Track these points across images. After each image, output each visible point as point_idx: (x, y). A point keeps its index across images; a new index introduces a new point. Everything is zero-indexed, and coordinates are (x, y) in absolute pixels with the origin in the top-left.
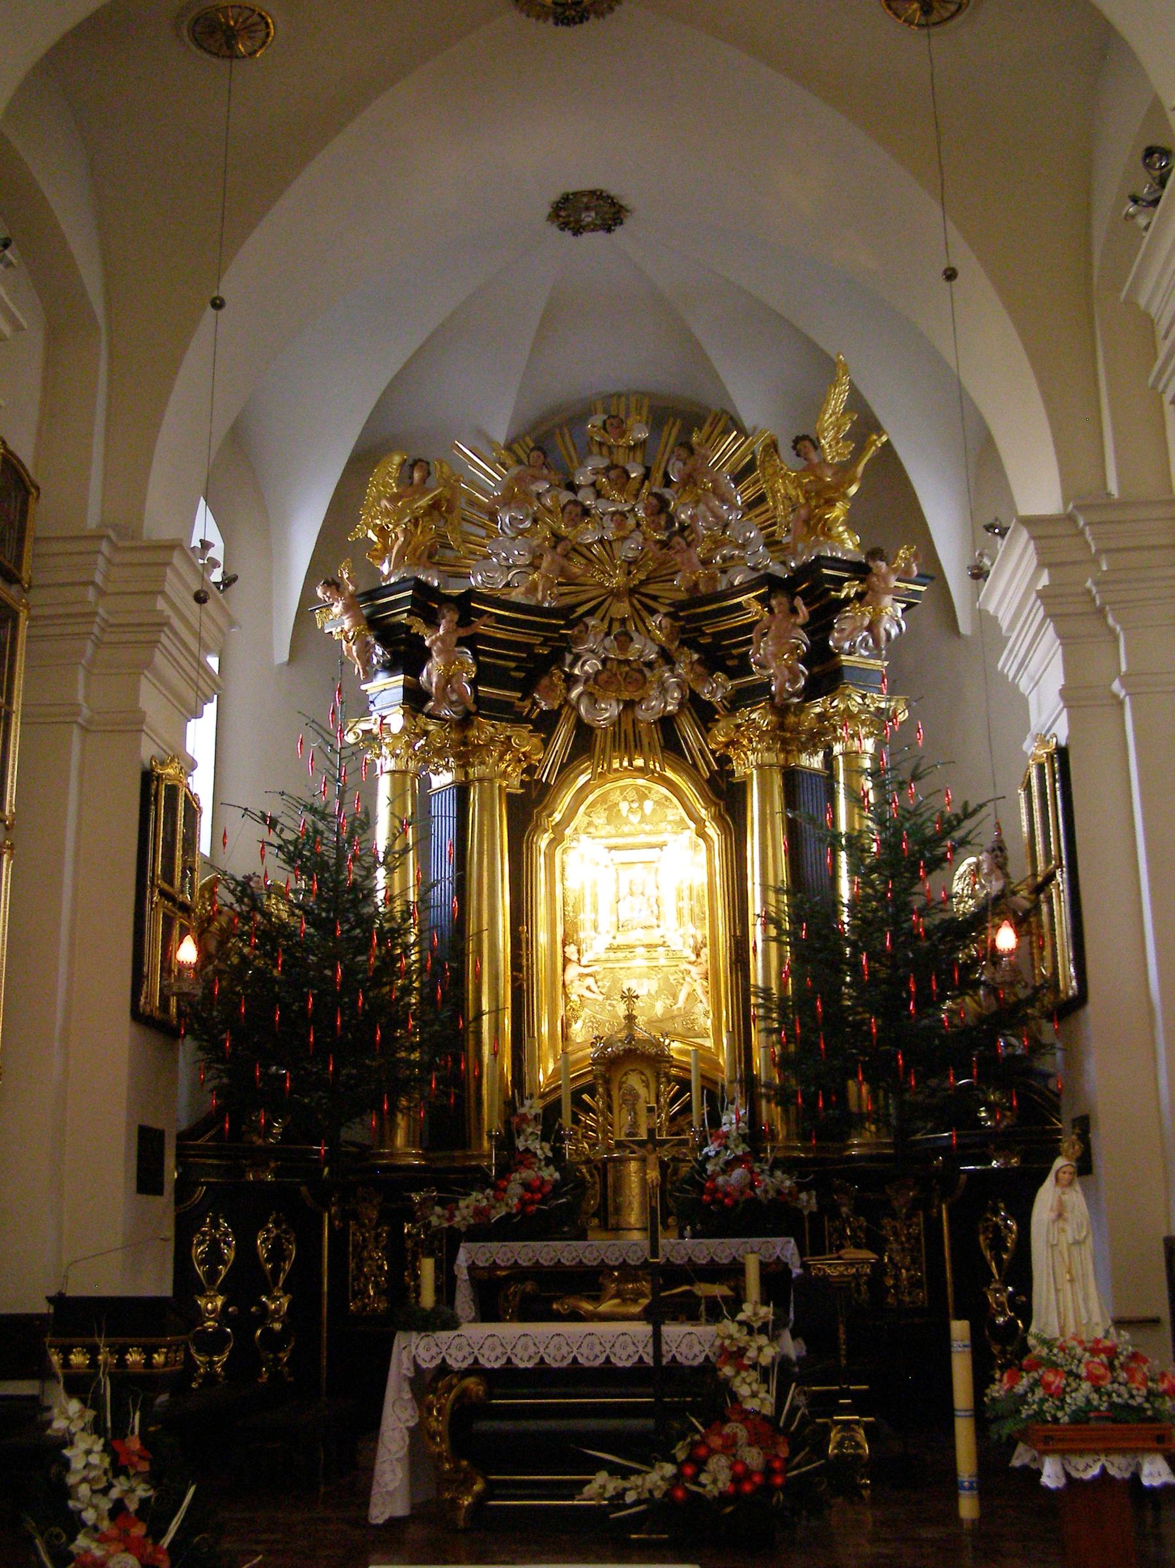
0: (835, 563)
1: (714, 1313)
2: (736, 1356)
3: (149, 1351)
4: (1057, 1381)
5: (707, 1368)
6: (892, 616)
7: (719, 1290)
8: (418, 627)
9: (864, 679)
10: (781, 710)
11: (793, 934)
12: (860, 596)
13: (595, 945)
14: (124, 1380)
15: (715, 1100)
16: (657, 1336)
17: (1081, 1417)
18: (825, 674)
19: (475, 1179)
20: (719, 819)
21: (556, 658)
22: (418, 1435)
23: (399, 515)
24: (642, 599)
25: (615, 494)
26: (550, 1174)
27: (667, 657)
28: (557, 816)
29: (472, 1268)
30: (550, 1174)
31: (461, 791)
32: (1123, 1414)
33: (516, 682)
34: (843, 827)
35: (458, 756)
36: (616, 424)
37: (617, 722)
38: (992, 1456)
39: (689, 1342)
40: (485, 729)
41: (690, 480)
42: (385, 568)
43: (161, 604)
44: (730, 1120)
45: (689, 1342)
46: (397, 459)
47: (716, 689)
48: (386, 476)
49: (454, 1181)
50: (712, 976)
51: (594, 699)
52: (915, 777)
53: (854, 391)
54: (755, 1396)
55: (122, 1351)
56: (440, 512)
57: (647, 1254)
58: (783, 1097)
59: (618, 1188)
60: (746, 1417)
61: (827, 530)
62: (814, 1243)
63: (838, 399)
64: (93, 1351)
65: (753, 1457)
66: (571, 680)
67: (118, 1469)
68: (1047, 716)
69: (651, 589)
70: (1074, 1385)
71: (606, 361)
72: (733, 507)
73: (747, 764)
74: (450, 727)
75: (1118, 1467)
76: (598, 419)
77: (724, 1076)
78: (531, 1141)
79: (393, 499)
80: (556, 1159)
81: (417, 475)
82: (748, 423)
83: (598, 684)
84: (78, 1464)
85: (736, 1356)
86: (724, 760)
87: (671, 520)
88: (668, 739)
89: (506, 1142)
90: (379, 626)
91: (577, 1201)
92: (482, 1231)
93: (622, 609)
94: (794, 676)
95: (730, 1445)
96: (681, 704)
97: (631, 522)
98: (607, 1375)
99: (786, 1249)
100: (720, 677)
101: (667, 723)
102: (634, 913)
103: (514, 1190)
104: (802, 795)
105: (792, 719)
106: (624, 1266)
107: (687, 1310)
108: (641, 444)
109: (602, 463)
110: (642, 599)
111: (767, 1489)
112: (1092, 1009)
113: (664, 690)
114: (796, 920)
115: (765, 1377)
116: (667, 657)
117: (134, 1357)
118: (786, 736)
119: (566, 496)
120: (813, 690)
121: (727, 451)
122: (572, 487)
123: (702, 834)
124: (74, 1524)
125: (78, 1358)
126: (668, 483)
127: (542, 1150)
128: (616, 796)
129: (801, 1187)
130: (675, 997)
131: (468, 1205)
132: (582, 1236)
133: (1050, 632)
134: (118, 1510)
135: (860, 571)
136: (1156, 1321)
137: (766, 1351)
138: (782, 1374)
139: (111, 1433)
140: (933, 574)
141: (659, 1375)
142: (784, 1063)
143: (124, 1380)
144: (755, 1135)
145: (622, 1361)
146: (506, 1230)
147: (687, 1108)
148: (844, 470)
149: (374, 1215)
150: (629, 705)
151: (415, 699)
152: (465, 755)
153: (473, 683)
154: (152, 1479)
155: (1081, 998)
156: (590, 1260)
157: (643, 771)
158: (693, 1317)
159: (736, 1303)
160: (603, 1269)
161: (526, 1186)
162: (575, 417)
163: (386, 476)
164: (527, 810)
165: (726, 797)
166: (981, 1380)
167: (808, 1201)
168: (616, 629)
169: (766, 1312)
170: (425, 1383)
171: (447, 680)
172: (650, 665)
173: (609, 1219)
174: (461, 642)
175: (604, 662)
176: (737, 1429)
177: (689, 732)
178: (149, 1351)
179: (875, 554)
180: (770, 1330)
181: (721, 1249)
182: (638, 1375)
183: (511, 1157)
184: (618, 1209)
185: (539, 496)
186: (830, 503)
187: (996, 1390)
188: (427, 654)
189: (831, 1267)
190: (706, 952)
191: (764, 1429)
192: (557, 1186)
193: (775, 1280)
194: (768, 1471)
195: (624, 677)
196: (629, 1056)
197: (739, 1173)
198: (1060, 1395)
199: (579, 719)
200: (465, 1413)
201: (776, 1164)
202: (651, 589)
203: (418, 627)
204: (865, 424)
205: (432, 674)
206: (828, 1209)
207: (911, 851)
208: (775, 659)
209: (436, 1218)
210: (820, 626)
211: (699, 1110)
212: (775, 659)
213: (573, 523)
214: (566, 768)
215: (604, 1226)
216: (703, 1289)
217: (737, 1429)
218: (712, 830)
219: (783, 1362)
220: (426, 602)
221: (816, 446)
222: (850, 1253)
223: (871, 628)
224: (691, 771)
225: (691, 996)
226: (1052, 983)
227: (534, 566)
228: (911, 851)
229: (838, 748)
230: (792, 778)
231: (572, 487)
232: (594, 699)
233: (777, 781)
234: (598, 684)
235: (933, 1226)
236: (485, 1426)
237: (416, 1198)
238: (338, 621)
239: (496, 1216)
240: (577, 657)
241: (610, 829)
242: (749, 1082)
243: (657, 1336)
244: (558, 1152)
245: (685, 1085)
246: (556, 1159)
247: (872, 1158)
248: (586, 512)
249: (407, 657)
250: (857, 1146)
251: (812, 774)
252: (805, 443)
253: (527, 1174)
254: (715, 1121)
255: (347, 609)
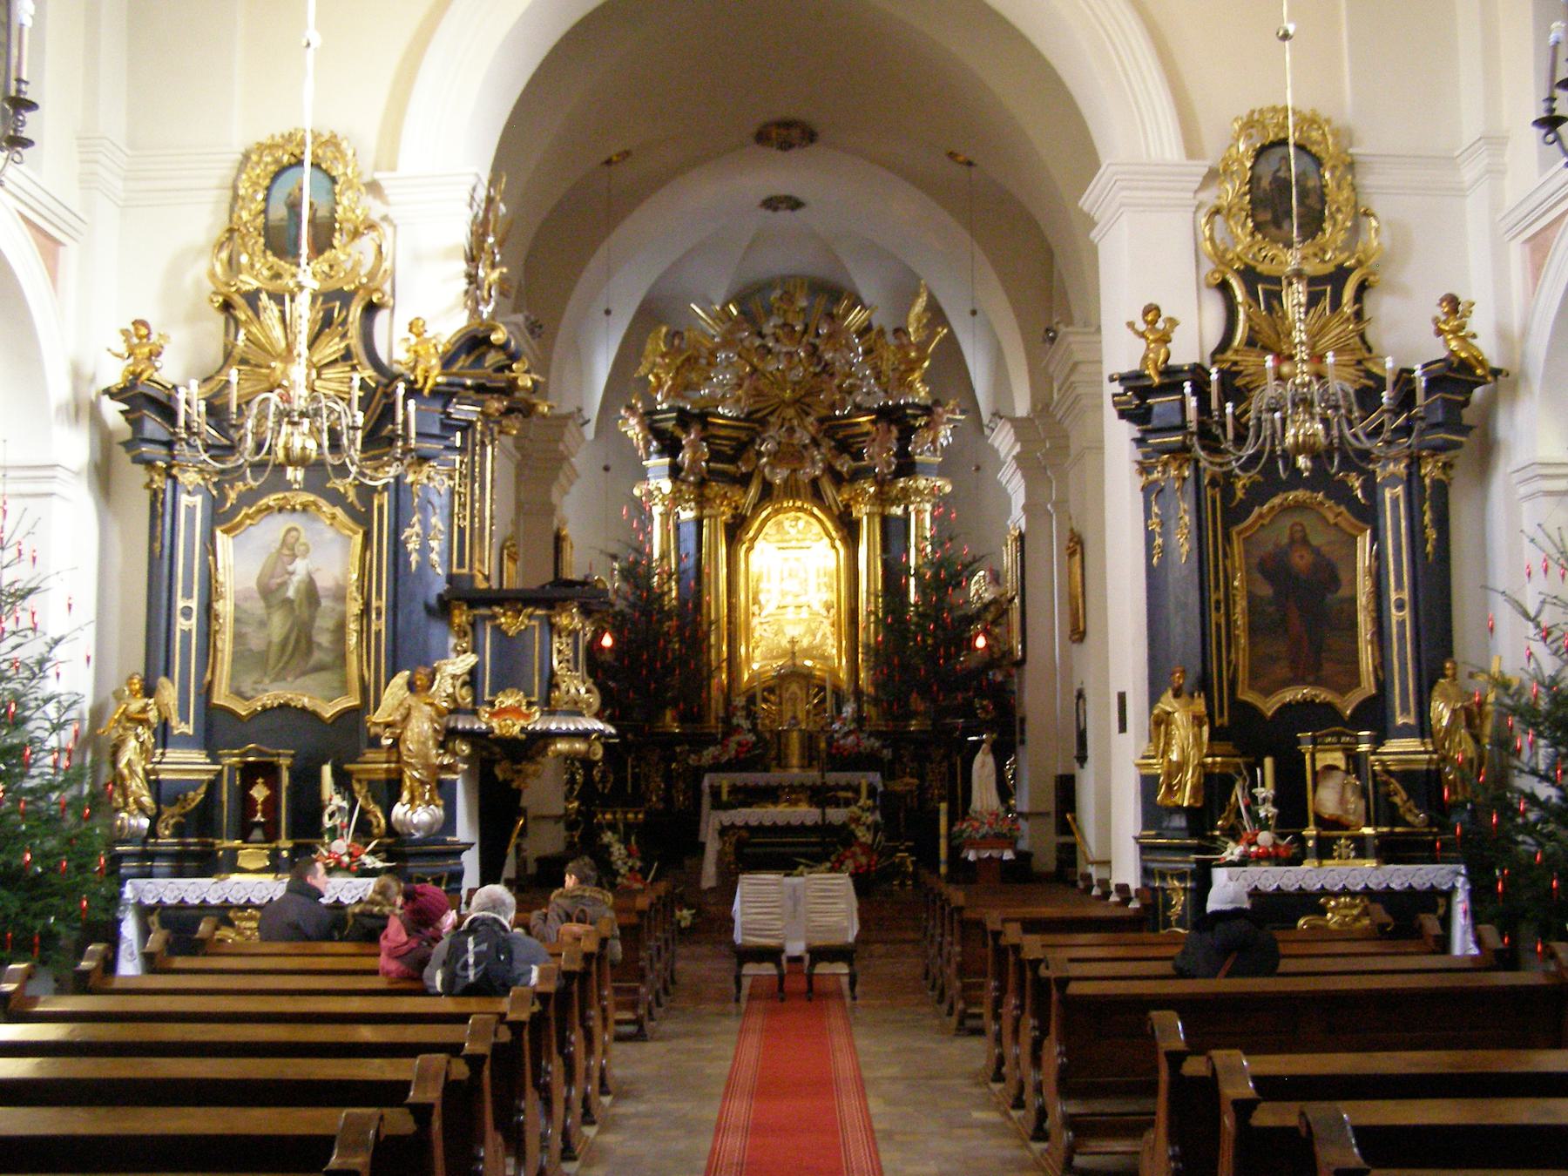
0: (915, 406)
1: (847, 803)
2: (857, 820)
3: (636, 814)
4: (976, 824)
5: (844, 826)
6: (945, 435)
7: (850, 795)
8: (678, 432)
9: (928, 470)
10: (880, 483)
11: (885, 618)
12: (927, 425)
13: (770, 608)
14: (628, 825)
15: (839, 703)
16: (824, 814)
17: (984, 837)
18: (907, 467)
19: (710, 740)
20: (844, 540)
21: (752, 441)
22: (721, 855)
23: (667, 368)
24: (802, 405)
25: (785, 341)
26: (751, 737)
27: (815, 443)
28: (751, 534)
29: (711, 786)
30: (751, 737)
31: (699, 522)
32: (998, 836)
33: (734, 469)
34: (912, 563)
35: (698, 503)
36: (788, 297)
37: (786, 481)
38: (955, 851)
39: (836, 815)
40: (715, 488)
41: (830, 336)
42: (659, 398)
43: (561, 447)
44: (848, 710)
45: (836, 815)
46: (664, 330)
47: (844, 465)
48: (657, 344)
49: (699, 741)
50: (836, 624)
51: (773, 467)
52: (951, 539)
53: (931, 297)
54: (864, 836)
55: (626, 813)
56: (690, 362)
57: (1338, 776)
58: (875, 701)
59: (787, 746)
60: (862, 845)
61: (911, 386)
62: (889, 774)
63: (921, 303)
64: (614, 813)
65: (863, 860)
66: (760, 455)
67: (630, 855)
68: (1017, 519)
69: (807, 400)
70: (236, 437)
71: (785, 257)
72: (857, 355)
73: (862, 511)
74: (697, 486)
75: (995, 853)
76: (778, 293)
77: (845, 687)
78: (740, 720)
79: (663, 356)
80: (754, 729)
81: (676, 342)
82: (867, 301)
83: (777, 458)
84: (616, 853)
85: (857, 820)
86: (848, 506)
87: (820, 359)
88: (817, 496)
89: (727, 720)
90: (653, 429)
91: (765, 752)
92: (717, 767)
93: (790, 412)
94: (889, 464)
95: (854, 855)
96: (824, 471)
97: (796, 359)
98: (802, 829)
99: (875, 778)
100: (847, 457)
101: (815, 482)
102: (793, 590)
103: (733, 746)
104: (893, 533)
105: (886, 488)
106: (791, 786)
107: (837, 803)
108: (803, 310)
109: (780, 321)
110: (802, 405)
111: (868, 872)
112: (1028, 667)
113: (814, 463)
114: (886, 613)
115: (868, 828)
116: (815, 443)
117: (630, 816)
118: (882, 499)
119: (758, 342)
120: (898, 474)
121: (856, 318)
122: (761, 335)
123: (834, 547)
124: (616, 873)
125: (608, 816)
126: (818, 335)
127: (746, 724)
128: (787, 524)
129: (884, 747)
130: (814, 636)
131: (709, 753)
132: (767, 769)
133: (1019, 475)
134: (631, 869)
135: (927, 410)
136: (1047, 814)
137: (869, 818)
138: (874, 828)
139: (625, 840)
140: (972, 408)
141: (824, 829)
142: (877, 685)
143: (628, 825)
144: (860, 719)
145: (809, 822)
146: (729, 767)
147: (823, 701)
148: (921, 347)
149: (656, 759)
150: (794, 471)
151: (675, 472)
152: (702, 501)
153: (707, 462)
154: (642, 859)
155: (1023, 660)
156: (774, 782)
157: (800, 509)
158: (838, 806)
159: (857, 801)
160: (780, 787)
161: (739, 744)
162: (763, 288)
163: (657, 344)
164: (736, 530)
165: (848, 528)
166: (951, 825)
167: (887, 753)
168: (787, 425)
169: (870, 802)
170: (724, 831)
171: (694, 461)
172: (805, 447)
173: (782, 762)
174: (703, 439)
175: (779, 443)
176: (857, 849)
177: (828, 489)
178: (636, 814)
179: (937, 403)
180: (871, 810)
181: (843, 777)
182: (815, 829)
183: (731, 730)
184: (786, 756)
185: (741, 341)
186: (912, 370)
187: (955, 829)
188: (681, 448)
189: (898, 786)
190: (833, 611)
191: (867, 849)
192: (754, 745)
193: (872, 792)
194: (869, 866)
195: (789, 455)
196: (793, 676)
197: (851, 738)
198: (977, 830)
199: (764, 478)
200: (740, 844)
201: (870, 735)
202: (807, 400)
203: (678, 432)
204: (936, 314)
205: (685, 457)
206: (897, 758)
207: (947, 576)
208: (880, 456)
209: (692, 760)
210: (904, 439)
211: (830, 703)
212: (880, 456)
213: (762, 358)
214: (757, 508)
215: (779, 765)
216: (842, 794)
217: (857, 849)
218: (838, 544)
219: (876, 824)
220: (684, 419)
221: (906, 333)
222: (908, 780)
223: (933, 442)
224: (827, 510)
225: (824, 635)
226: (1011, 651)
227: (740, 386)
228: (947, 576)
229: (911, 508)
230: (886, 521)
231: (761, 335)
232: (773, 467)
233: (877, 520)
234: (777, 458)
235: (952, 766)
236: (747, 850)
237: (678, 749)
238: (633, 429)
239: (725, 758)
240: (763, 441)
241: (778, 537)
242: (858, 693)
243: (824, 814)
244: (755, 725)
245: (822, 688)
246: (754, 729)
247: (920, 732)
248: (769, 351)
249: (670, 447)
250: (913, 726)
251: (897, 518)
252: (900, 331)
253: (736, 738)
254: (839, 711)
255: (641, 423)
